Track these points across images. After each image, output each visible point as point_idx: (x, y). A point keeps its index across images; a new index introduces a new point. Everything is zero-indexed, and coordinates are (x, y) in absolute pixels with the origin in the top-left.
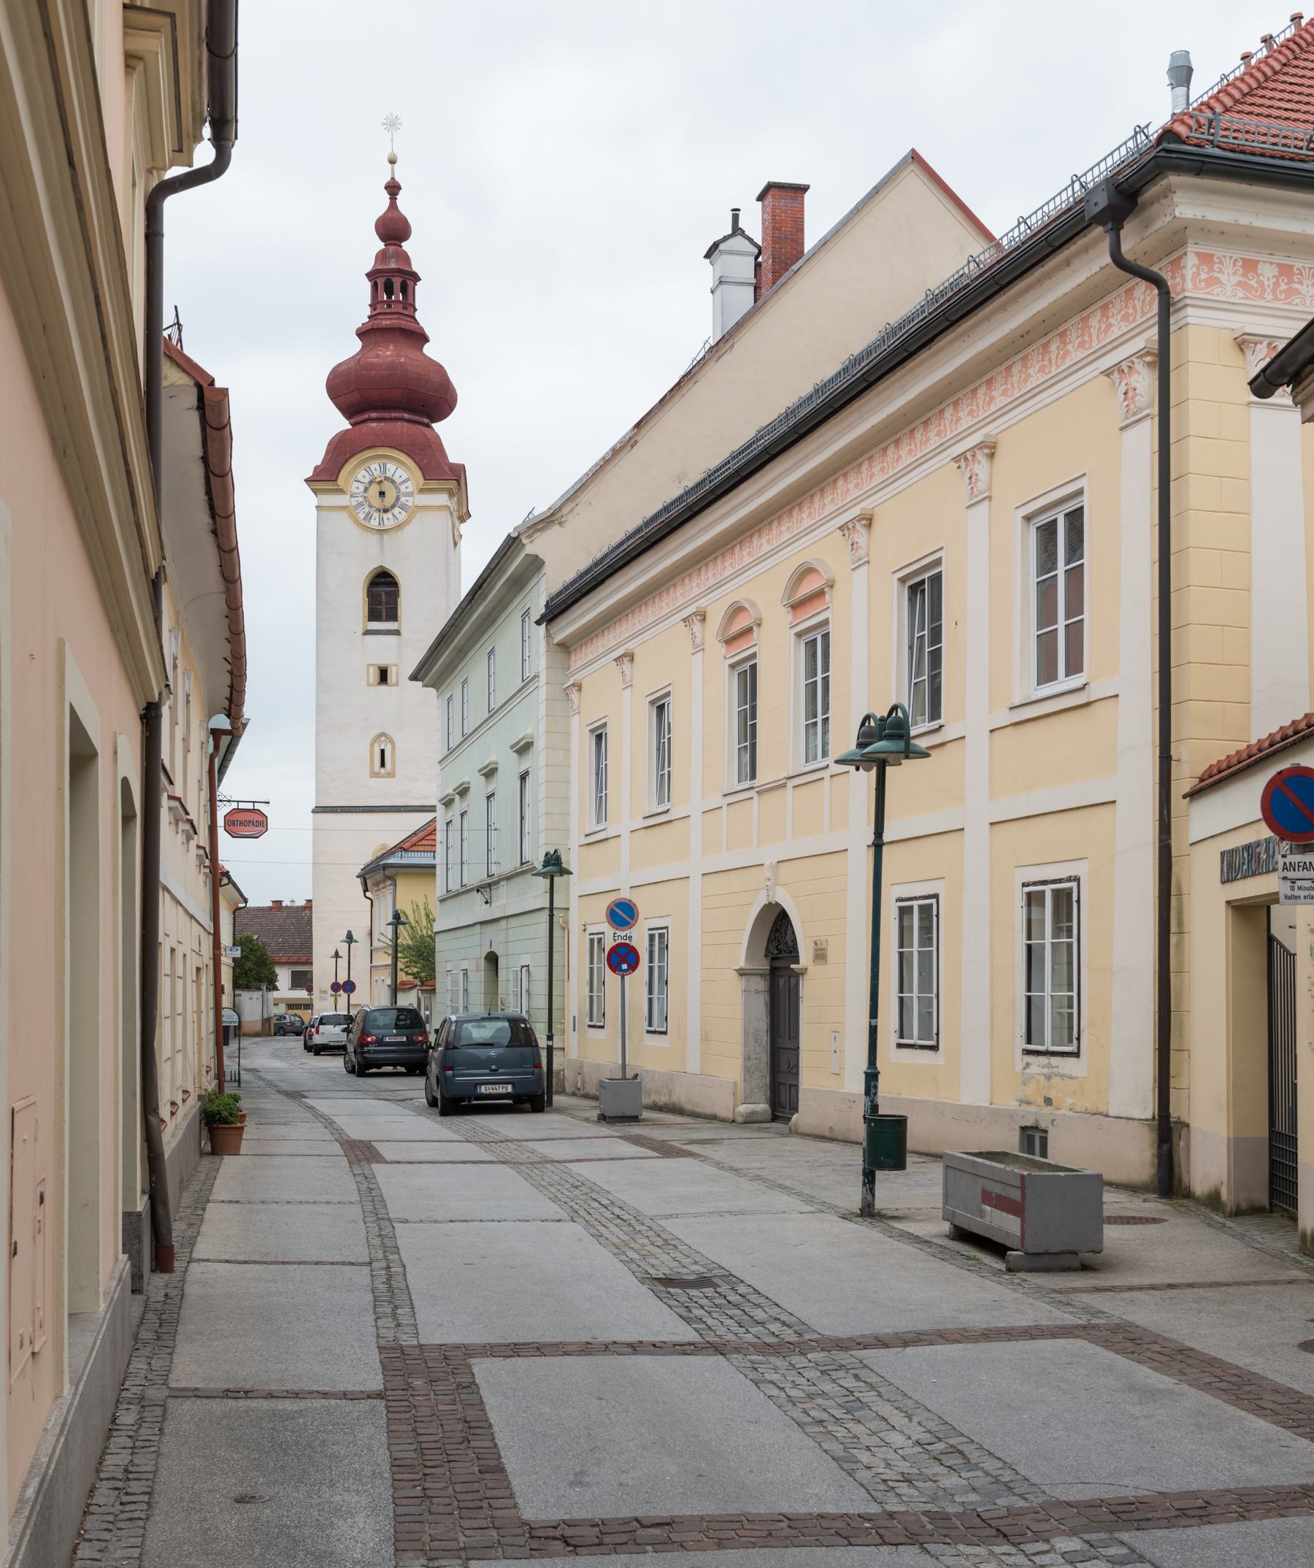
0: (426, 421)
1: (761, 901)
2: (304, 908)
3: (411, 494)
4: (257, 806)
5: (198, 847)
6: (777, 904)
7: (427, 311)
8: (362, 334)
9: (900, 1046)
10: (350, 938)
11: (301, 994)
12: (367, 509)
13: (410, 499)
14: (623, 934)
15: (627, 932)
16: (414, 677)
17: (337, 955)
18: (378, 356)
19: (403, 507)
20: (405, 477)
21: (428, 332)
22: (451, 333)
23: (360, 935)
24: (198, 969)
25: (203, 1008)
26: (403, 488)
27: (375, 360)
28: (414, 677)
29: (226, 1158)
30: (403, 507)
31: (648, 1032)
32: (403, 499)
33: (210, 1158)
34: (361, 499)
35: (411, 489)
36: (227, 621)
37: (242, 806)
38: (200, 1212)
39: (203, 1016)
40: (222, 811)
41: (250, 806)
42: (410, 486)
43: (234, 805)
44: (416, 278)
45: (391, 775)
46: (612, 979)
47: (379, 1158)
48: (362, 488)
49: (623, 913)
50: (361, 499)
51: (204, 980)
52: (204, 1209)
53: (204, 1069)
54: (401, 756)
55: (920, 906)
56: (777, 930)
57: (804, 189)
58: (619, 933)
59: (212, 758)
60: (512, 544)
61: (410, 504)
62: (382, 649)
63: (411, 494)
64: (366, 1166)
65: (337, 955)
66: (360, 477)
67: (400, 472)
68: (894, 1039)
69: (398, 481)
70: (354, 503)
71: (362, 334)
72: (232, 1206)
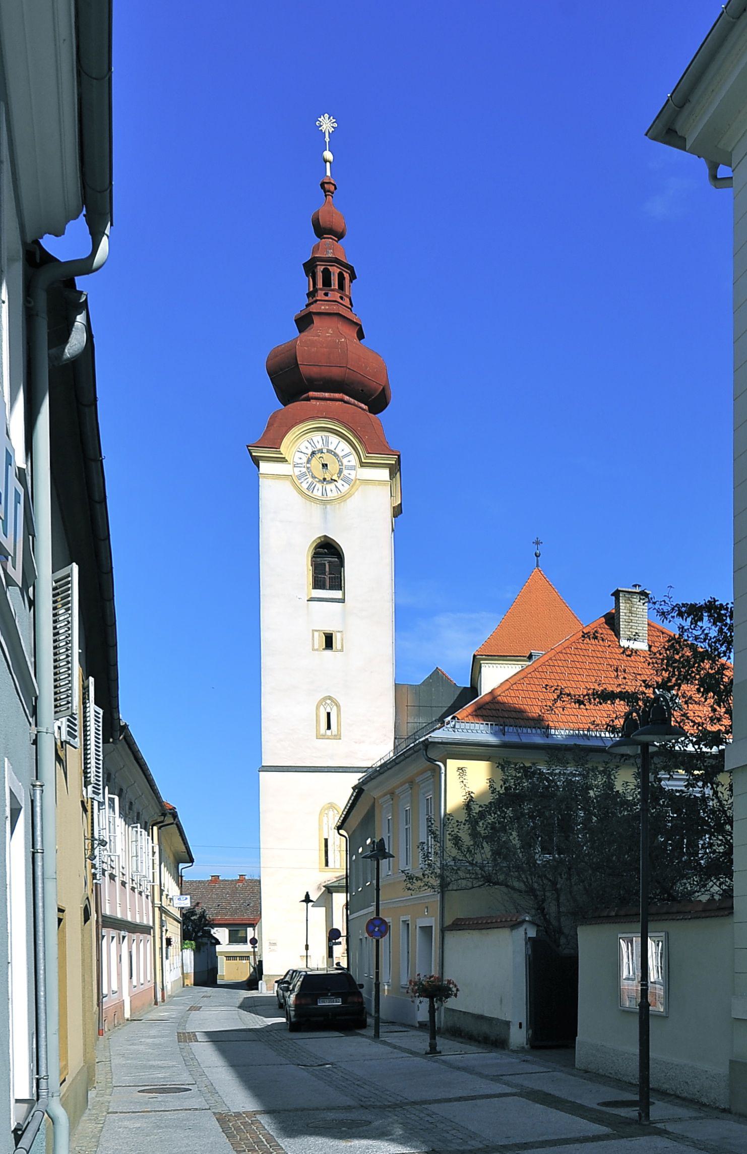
12: (310, 480)
19: (346, 480)
30: (346, 480)
34: (304, 470)
45: (338, 737)
48: (305, 460)
50: (304, 470)
54: (346, 719)
61: (352, 477)
63: (353, 468)
69: (341, 454)
70: (297, 473)
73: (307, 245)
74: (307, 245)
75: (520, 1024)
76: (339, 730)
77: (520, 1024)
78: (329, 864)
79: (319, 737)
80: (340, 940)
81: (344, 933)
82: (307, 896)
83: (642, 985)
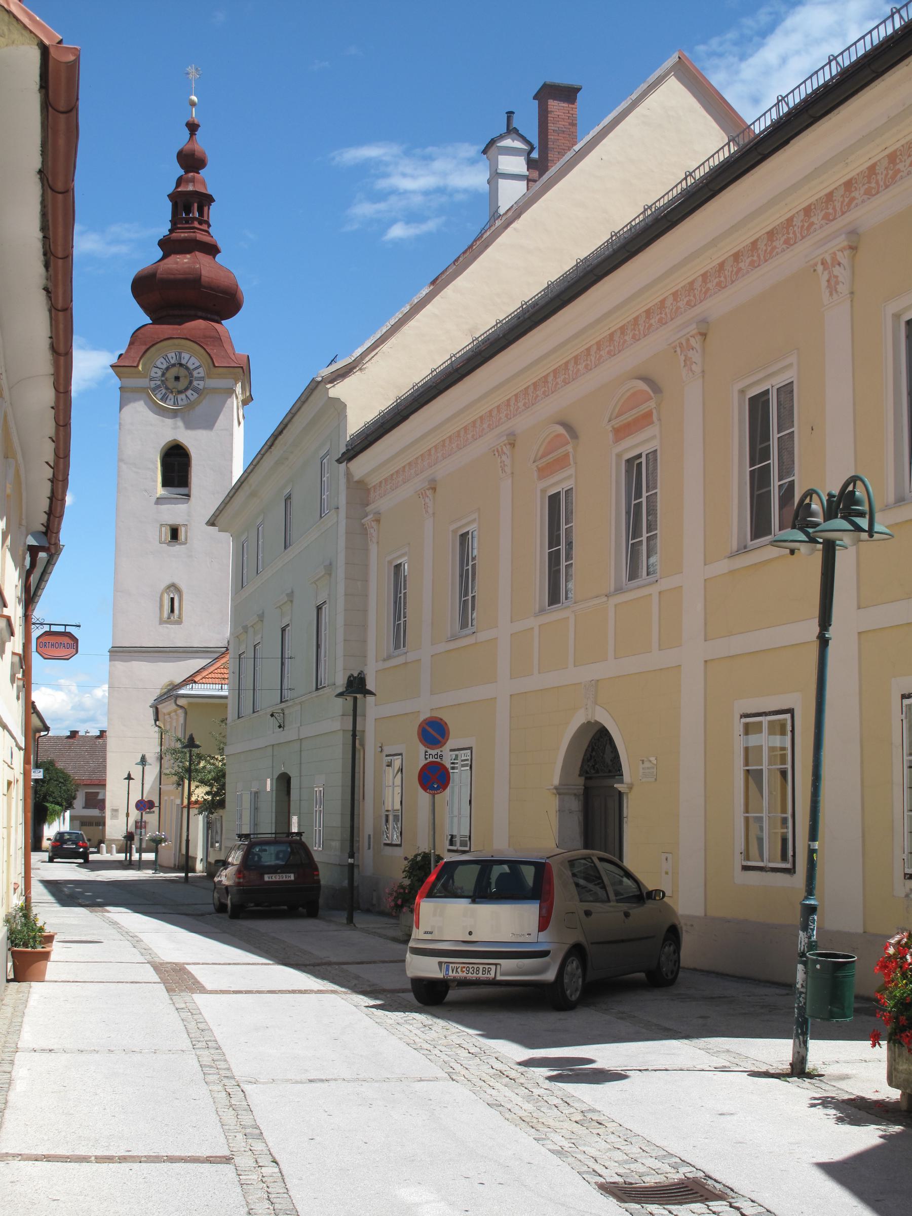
0: (216, 318)
1: (578, 720)
2: (98, 737)
3: (202, 379)
4: (69, 629)
5: (14, 654)
6: (597, 723)
7: (220, 224)
8: (163, 243)
9: (745, 868)
10: (143, 761)
11: (95, 812)
12: (164, 391)
13: (201, 383)
14: (434, 752)
15: (438, 751)
16: (211, 523)
17: (129, 778)
18: (177, 263)
19: (196, 390)
20: (197, 364)
21: (220, 245)
22: (238, 250)
23: (152, 758)
24: (9, 783)
25: (13, 823)
26: (195, 373)
27: (175, 266)
28: (211, 523)
29: (33, 984)
30: (196, 390)
31: (449, 851)
32: (195, 383)
33: (14, 985)
34: (159, 383)
35: (202, 375)
36: (53, 411)
37: (54, 629)
38: (7, 1068)
39: (13, 830)
40: (36, 633)
41: (61, 629)
42: (201, 372)
43: (47, 628)
44: (209, 199)
45: (179, 621)
46: (424, 797)
47: (197, 987)
48: (160, 373)
49: (434, 732)
50: (159, 383)
51: (14, 794)
52: (12, 1062)
53: (12, 887)
54: (189, 606)
55: (769, 722)
56: (593, 750)
57: (578, 90)
58: (430, 751)
59: (29, 573)
60: (314, 386)
61: (201, 387)
62: (175, 513)
63: (202, 379)
64: (187, 999)
65: (129, 778)
66: (158, 364)
67: (193, 360)
68: (98, 855)
69: (191, 367)
70: (153, 386)
71: (163, 243)
72: (46, 1055)
73: (182, 138)
74: (182, 138)
75: (431, 933)
76: (180, 617)
77: (431, 933)
78: (575, 585)
79: (162, 622)
80: (154, 809)
81: (157, 804)
82: (129, 775)
83: (486, 865)
